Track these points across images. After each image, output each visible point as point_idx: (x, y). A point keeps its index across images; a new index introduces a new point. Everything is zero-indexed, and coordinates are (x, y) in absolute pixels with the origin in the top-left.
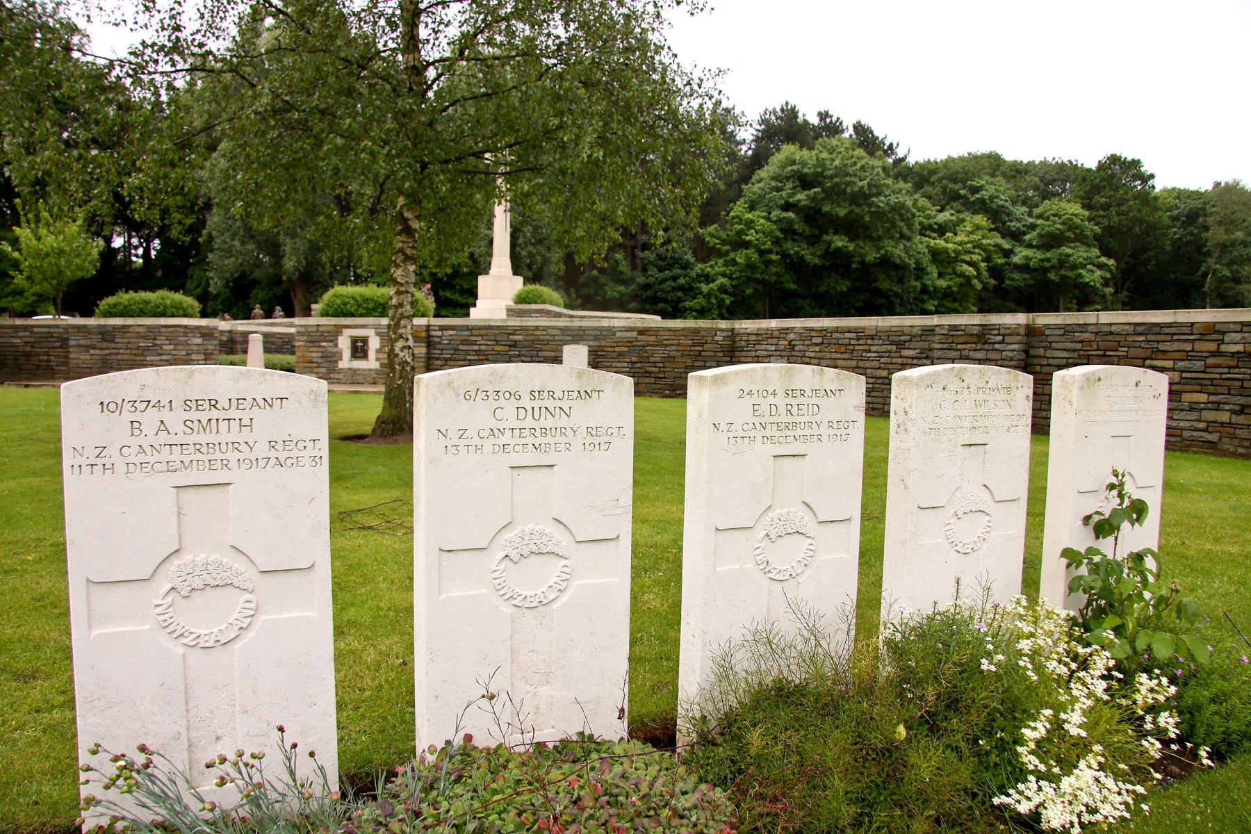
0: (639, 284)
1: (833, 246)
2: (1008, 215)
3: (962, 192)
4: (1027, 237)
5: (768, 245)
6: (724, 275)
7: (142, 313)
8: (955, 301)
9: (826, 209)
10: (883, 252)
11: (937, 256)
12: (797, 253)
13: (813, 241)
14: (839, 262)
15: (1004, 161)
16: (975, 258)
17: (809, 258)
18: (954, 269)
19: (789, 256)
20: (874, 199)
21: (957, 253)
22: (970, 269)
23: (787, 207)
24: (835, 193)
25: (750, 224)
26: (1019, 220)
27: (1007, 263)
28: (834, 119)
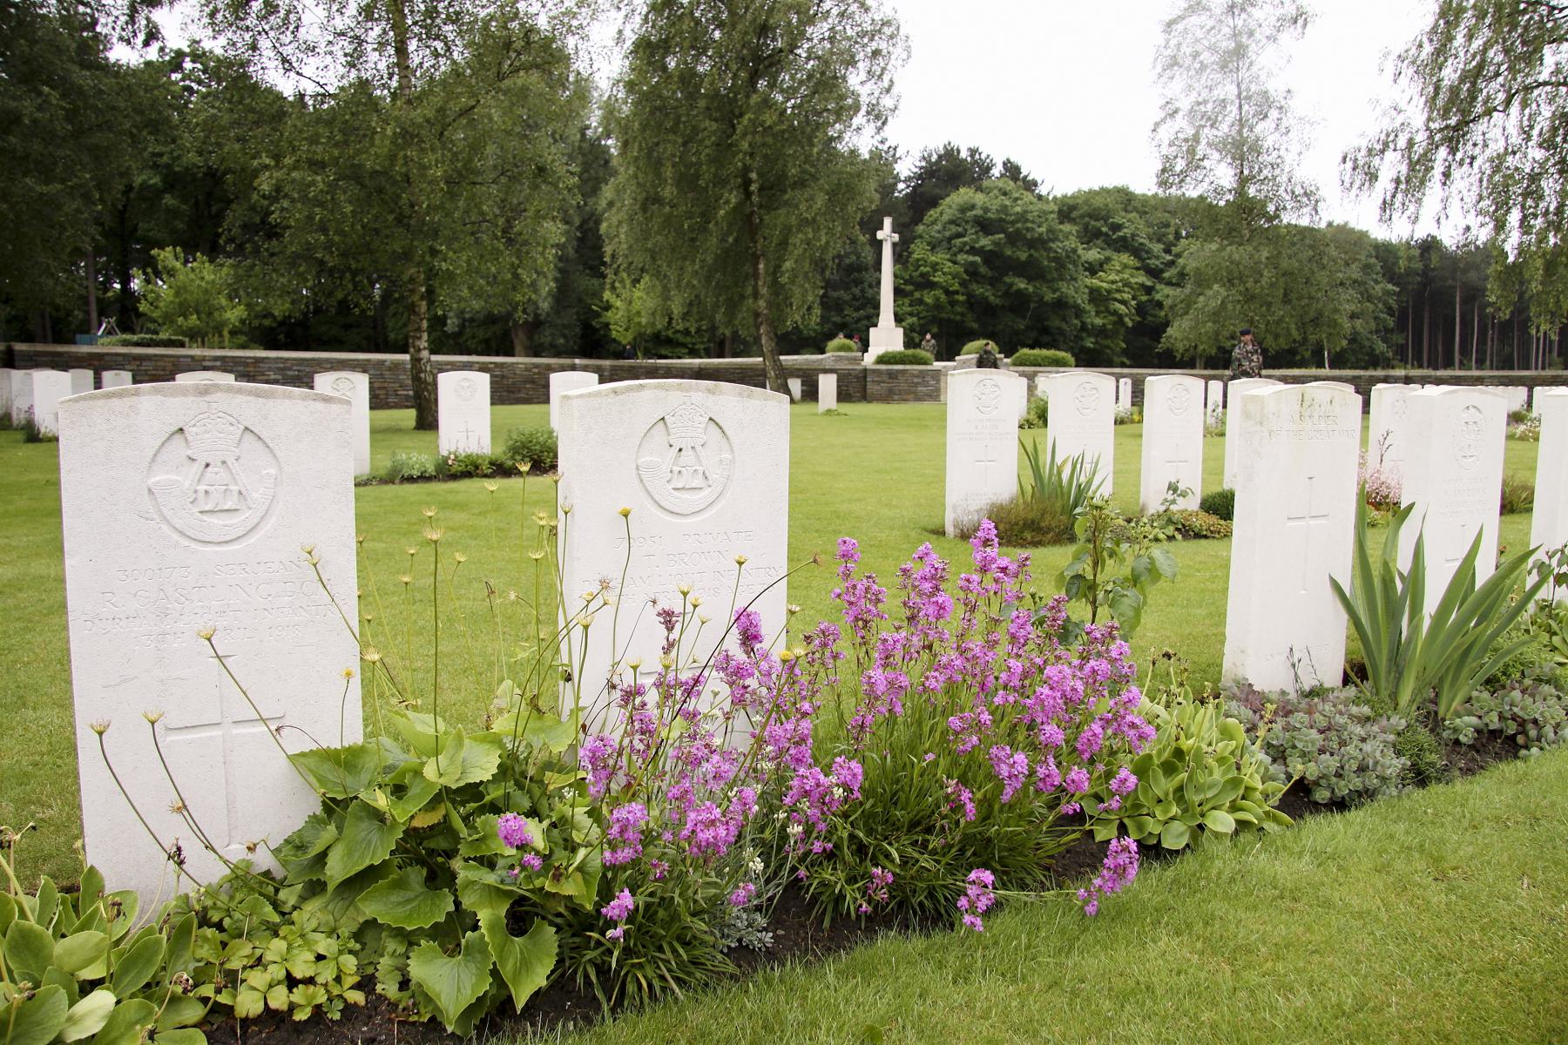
0: (834, 323)
1: (1015, 288)
2: (1147, 252)
3: (1104, 229)
4: (1166, 275)
5: (956, 287)
6: (911, 314)
7: (148, 345)
8: (1107, 337)
9: (1008, 252)
10: (1058, 294)
11: (1096, 296)
12: (982, 294)
13: (993, 282)
14: (1019, 302)
15: (1136, 196)
16: (1126, 296)
17: (992, 298)
18: (1107, 308)
19: (973, 296)
20: (1051, 245)
21: (1109, 292)
22: (1123, 307)
23: (973, 251)
24: (1014, 239)
25: (935, 266)
26: (1157, 258)
27: (1149, 301)
28: (983, 157)
